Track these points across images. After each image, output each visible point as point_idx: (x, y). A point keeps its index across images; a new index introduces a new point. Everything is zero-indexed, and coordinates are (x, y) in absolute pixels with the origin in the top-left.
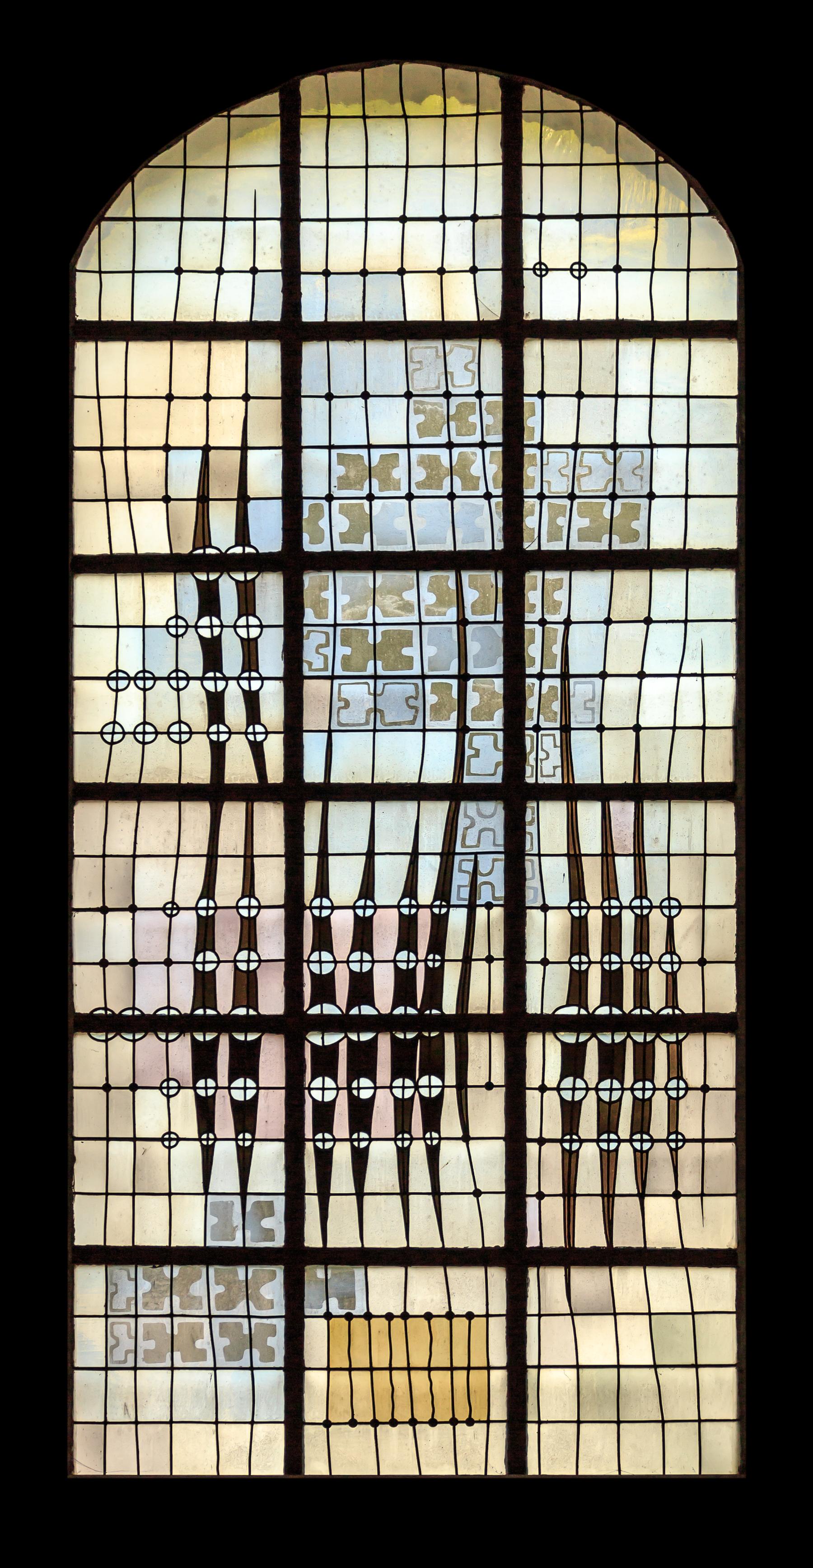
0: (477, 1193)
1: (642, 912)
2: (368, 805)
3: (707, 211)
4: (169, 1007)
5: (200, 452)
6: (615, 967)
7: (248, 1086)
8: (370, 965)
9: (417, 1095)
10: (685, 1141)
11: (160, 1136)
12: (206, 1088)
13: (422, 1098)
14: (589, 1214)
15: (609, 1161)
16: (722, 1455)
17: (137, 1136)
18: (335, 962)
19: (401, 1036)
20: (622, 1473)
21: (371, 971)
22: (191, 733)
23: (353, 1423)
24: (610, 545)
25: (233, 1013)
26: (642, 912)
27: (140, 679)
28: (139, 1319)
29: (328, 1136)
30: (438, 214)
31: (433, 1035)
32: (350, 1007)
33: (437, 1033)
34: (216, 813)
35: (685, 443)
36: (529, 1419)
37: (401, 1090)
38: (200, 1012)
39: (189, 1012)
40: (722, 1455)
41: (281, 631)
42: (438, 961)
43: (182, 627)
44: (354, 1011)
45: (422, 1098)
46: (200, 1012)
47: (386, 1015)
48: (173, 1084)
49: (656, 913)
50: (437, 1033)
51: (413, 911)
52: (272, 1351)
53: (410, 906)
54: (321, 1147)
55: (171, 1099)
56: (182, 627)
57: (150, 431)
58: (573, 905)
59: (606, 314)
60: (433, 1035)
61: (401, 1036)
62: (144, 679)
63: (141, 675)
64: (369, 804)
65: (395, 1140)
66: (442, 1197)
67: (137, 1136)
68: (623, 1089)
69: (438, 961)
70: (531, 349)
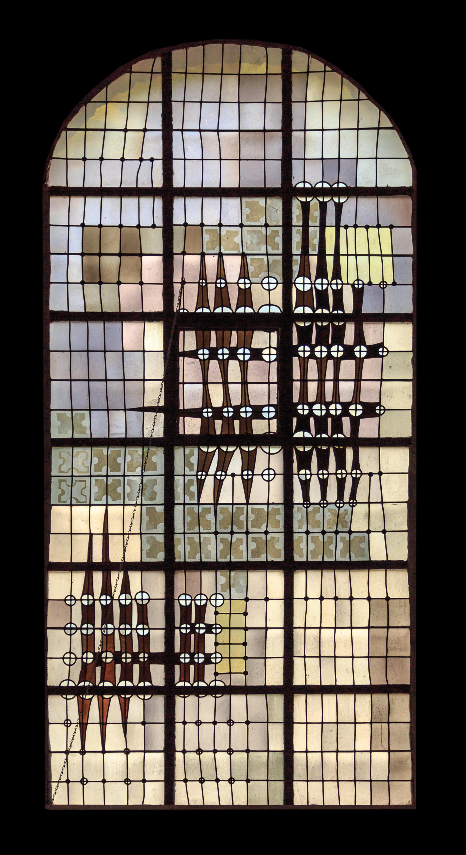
2: (51, 353)
8: (341, 286)
9: (331, 311)
13: (327, 279)
17: (108, 378)
20: (48, 660)
21: (342, 288)
22: (262, 475)
23: (245, 614)
28: (186, 535)
32: (332, 434)
35: (87, 379)
36: (276, 385)
37: (271, 356)
41: (280, 105)
44: (335, 436)
45: (327, 279)
47: (192, 313)
52: (155, 464)
58: (121, 627)
66: (340, 383)
67: (108, 378)
68: (132, 629)
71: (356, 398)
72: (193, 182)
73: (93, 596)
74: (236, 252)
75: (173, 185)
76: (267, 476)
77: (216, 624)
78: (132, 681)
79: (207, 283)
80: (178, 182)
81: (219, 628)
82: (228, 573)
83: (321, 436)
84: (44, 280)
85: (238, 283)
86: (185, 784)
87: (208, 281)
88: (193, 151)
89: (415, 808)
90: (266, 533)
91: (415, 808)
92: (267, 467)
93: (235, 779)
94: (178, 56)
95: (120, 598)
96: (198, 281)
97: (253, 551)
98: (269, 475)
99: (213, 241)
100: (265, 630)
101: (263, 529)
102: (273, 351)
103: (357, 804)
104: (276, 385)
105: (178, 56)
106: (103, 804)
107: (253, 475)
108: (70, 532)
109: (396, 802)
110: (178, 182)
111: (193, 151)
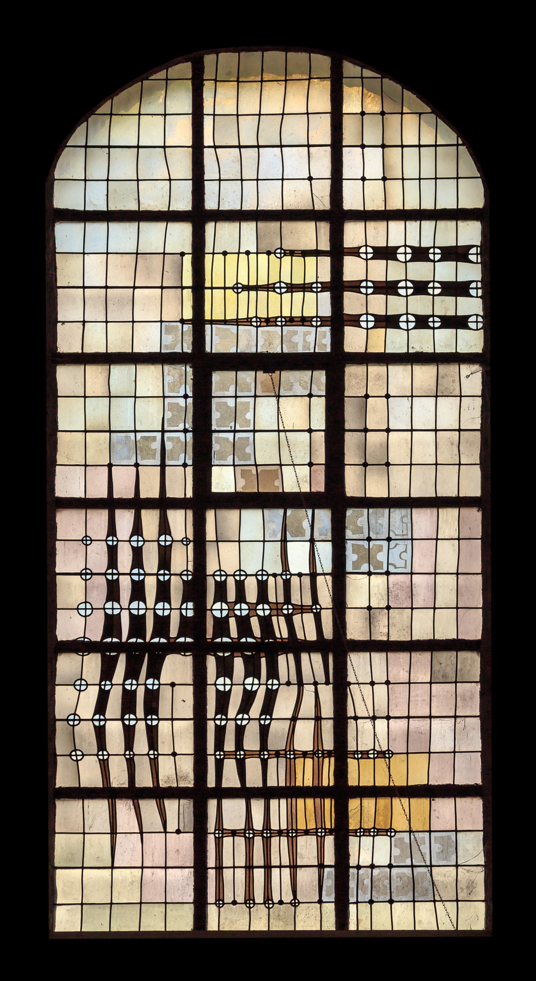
0: (174, 754)
3: (86, 123)
4: (84, 637)
7: (226, 686)
10: (80, 720)
15: (129, 733)
16: (474, 917)
18: (129, 609)
24: (315, 350)
25: (152, 641)
29: (132, 716)
31: (226, 655)
33: (229, 654)
34: (138, 519)
39: (99, 639)
40: (474, 917)
49: (271, 580)
50: (229, 654)
51: (142, 577)
53: (139, 574)
54: (150, 724)
57: (106, 288)
58: (160, 572)
59: (275, 206)
60: (226, 655)
65: (119, 574)
70: (210, 227)
72: (230, 203)
74: (280, 470)
75: (204, 207)
76: (87, 610)
77: (281, 294)
78: (229, 636)
80: (210, 204)
81: (265, 575)
82: (184, 368)
84: (390, 936)
88: (230, 169)
93: (290, 905)
94: (209, 59)
96: (273, 722)
100: (132, 289)
102: (480, 319)
105: (209, 59)
107: (123, 685)
110: (210, 204)
111: (230, 169)
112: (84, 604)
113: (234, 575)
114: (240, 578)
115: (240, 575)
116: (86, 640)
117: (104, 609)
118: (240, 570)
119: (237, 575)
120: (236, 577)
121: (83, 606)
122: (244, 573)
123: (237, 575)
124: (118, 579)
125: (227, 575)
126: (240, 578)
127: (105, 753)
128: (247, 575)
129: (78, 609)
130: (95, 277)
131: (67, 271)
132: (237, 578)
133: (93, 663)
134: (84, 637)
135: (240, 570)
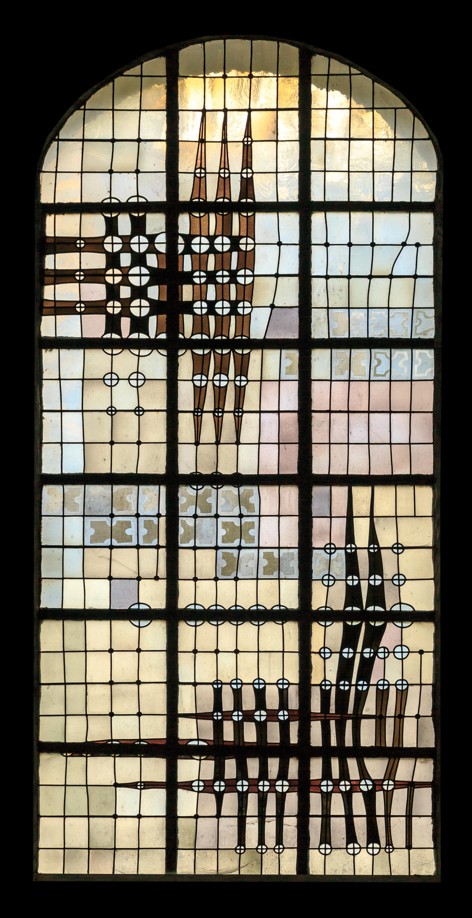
1: (351, 546)
5: (117, 789)
6: (350, 577)
11: (133, 409)
12: (353, 580)
14: (361, 506)
19: (349, 623)
26: (351, 546)
27: (395, 548)
30: (136, 137)
38: (244, 200)
39: (341, 608)
42: (347, 685)
43: (402, 580)
46: (244, 200)
48: (327, 650)
55: (326, 660)
56: (402, 580)
61: (349, 623)
62: (398, 548)
63: (396, 546)
64: (312, 246)
65: (356, 548)
69: (347, 685)
71: (219, 797)
73: (235, 385)
79: (141, 782)
83: (247, 200)
85: (248, 381)
86: (141, 711)
87: (139, 780)
89: (439, 880)
90: (112, 516)
91: (439, 880)
92: (120, 378)
95: (251, 309)
97: (144, 537)
98: (111, 379)
99: (420, 855)
101: (115, 519)
103: (433, 306)
104: (296, 687)
106: (276, 201)
108: (278, 171)
109: (429, 644)
112: (110, 375)
113: (396, 685)
114: (259, 687)
115: (402, 685)
116: (327, 609)
117: (252, 307)
118: (259, 679)
119: (280, 684)
120: (255, 686)
121: (109, 376)
122: (329, 683)
123: (280, 684)
124: (346, 545)
125: (389, 685)
126: (259, 687)
127: (356, 846)
128: (242, 684)
129: (104, 379)
130: (400, 421)
131: (424, 428)
132: (281, 686)
133: (263, 192)
134: (326, 607)
135: (259, 679)
